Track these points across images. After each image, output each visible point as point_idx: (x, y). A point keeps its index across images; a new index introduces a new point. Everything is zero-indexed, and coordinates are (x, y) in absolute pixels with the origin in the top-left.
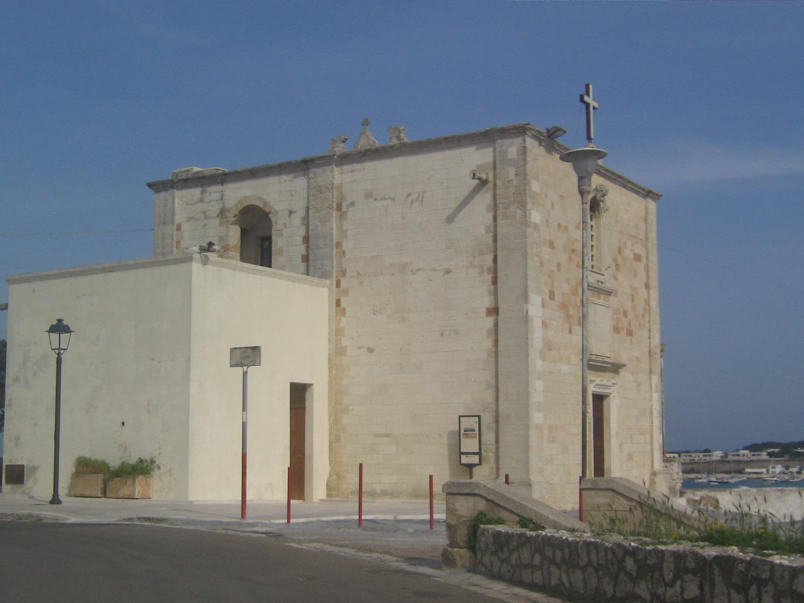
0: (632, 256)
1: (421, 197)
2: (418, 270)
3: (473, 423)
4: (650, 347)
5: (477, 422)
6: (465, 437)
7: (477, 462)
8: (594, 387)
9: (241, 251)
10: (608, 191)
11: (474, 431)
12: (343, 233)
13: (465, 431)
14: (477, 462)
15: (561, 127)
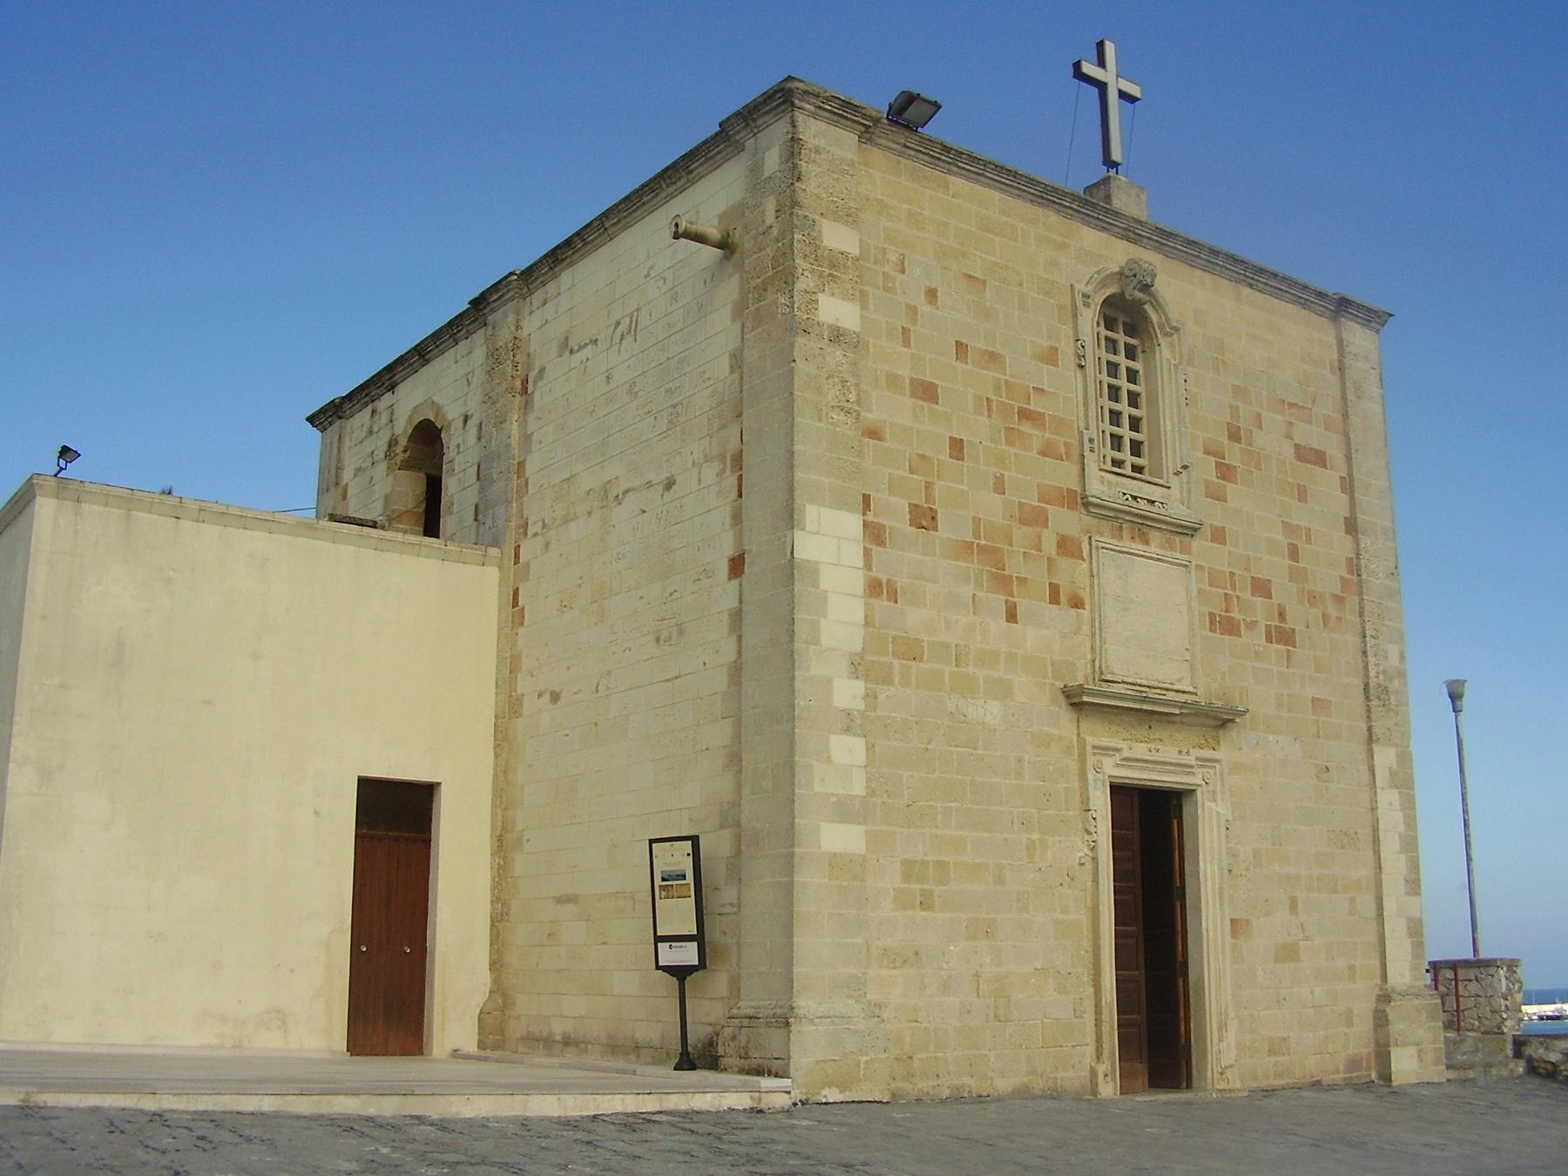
0: (1290, 452)
1: (634, 319)
2: (626, 492)
3: (677, 858)
4: (1367, 675)
5: (689, 854)
6: (663, 893)
7: (694, 960)
8: (1117, 765)
9: (425, 523)
10: (1154, 276)
11: (684, 877)
12: (527, 438)
13: (663, 880)
14: (694, 960)
15: (915, 91)
